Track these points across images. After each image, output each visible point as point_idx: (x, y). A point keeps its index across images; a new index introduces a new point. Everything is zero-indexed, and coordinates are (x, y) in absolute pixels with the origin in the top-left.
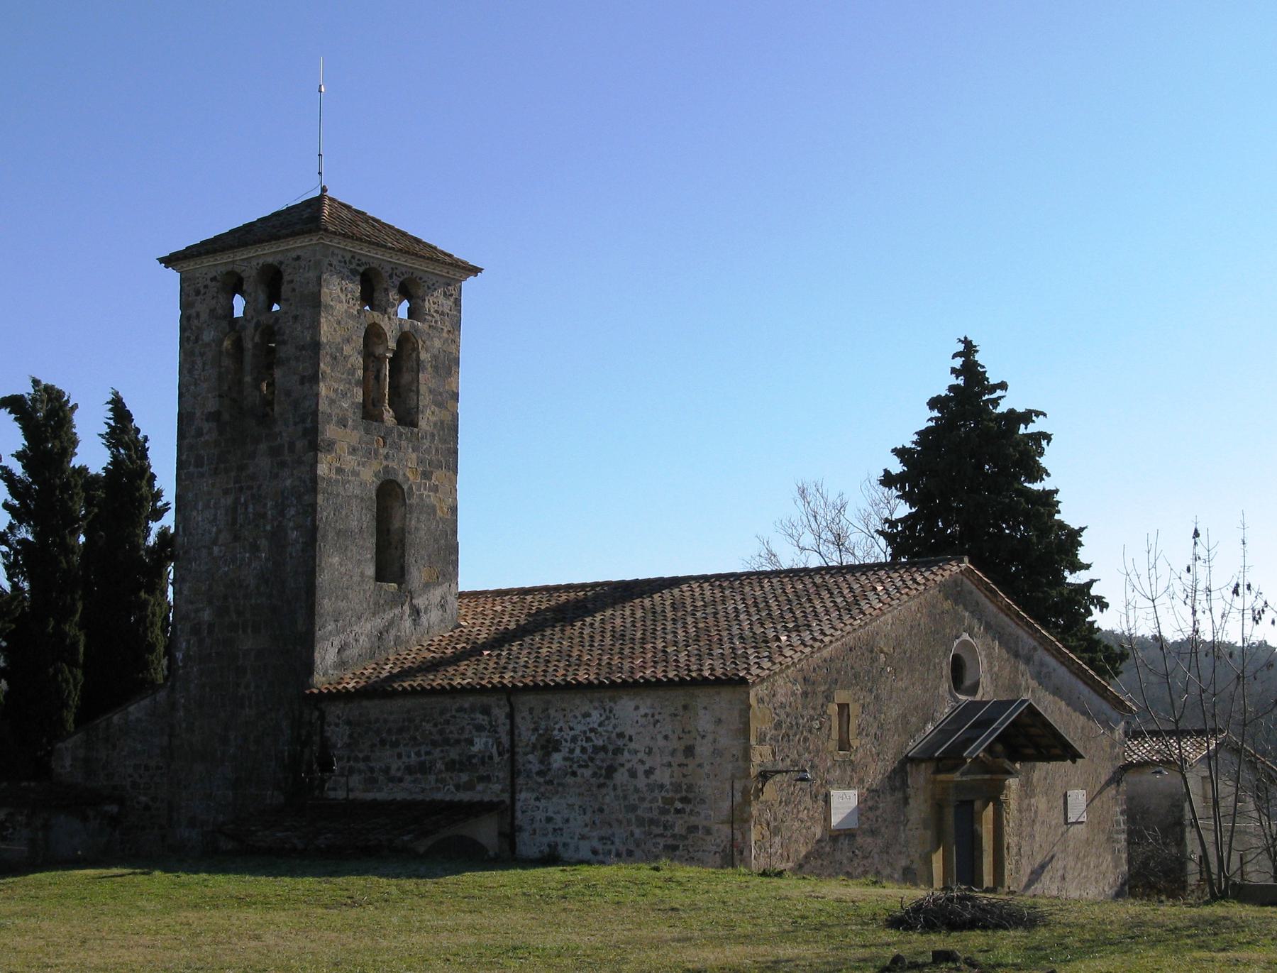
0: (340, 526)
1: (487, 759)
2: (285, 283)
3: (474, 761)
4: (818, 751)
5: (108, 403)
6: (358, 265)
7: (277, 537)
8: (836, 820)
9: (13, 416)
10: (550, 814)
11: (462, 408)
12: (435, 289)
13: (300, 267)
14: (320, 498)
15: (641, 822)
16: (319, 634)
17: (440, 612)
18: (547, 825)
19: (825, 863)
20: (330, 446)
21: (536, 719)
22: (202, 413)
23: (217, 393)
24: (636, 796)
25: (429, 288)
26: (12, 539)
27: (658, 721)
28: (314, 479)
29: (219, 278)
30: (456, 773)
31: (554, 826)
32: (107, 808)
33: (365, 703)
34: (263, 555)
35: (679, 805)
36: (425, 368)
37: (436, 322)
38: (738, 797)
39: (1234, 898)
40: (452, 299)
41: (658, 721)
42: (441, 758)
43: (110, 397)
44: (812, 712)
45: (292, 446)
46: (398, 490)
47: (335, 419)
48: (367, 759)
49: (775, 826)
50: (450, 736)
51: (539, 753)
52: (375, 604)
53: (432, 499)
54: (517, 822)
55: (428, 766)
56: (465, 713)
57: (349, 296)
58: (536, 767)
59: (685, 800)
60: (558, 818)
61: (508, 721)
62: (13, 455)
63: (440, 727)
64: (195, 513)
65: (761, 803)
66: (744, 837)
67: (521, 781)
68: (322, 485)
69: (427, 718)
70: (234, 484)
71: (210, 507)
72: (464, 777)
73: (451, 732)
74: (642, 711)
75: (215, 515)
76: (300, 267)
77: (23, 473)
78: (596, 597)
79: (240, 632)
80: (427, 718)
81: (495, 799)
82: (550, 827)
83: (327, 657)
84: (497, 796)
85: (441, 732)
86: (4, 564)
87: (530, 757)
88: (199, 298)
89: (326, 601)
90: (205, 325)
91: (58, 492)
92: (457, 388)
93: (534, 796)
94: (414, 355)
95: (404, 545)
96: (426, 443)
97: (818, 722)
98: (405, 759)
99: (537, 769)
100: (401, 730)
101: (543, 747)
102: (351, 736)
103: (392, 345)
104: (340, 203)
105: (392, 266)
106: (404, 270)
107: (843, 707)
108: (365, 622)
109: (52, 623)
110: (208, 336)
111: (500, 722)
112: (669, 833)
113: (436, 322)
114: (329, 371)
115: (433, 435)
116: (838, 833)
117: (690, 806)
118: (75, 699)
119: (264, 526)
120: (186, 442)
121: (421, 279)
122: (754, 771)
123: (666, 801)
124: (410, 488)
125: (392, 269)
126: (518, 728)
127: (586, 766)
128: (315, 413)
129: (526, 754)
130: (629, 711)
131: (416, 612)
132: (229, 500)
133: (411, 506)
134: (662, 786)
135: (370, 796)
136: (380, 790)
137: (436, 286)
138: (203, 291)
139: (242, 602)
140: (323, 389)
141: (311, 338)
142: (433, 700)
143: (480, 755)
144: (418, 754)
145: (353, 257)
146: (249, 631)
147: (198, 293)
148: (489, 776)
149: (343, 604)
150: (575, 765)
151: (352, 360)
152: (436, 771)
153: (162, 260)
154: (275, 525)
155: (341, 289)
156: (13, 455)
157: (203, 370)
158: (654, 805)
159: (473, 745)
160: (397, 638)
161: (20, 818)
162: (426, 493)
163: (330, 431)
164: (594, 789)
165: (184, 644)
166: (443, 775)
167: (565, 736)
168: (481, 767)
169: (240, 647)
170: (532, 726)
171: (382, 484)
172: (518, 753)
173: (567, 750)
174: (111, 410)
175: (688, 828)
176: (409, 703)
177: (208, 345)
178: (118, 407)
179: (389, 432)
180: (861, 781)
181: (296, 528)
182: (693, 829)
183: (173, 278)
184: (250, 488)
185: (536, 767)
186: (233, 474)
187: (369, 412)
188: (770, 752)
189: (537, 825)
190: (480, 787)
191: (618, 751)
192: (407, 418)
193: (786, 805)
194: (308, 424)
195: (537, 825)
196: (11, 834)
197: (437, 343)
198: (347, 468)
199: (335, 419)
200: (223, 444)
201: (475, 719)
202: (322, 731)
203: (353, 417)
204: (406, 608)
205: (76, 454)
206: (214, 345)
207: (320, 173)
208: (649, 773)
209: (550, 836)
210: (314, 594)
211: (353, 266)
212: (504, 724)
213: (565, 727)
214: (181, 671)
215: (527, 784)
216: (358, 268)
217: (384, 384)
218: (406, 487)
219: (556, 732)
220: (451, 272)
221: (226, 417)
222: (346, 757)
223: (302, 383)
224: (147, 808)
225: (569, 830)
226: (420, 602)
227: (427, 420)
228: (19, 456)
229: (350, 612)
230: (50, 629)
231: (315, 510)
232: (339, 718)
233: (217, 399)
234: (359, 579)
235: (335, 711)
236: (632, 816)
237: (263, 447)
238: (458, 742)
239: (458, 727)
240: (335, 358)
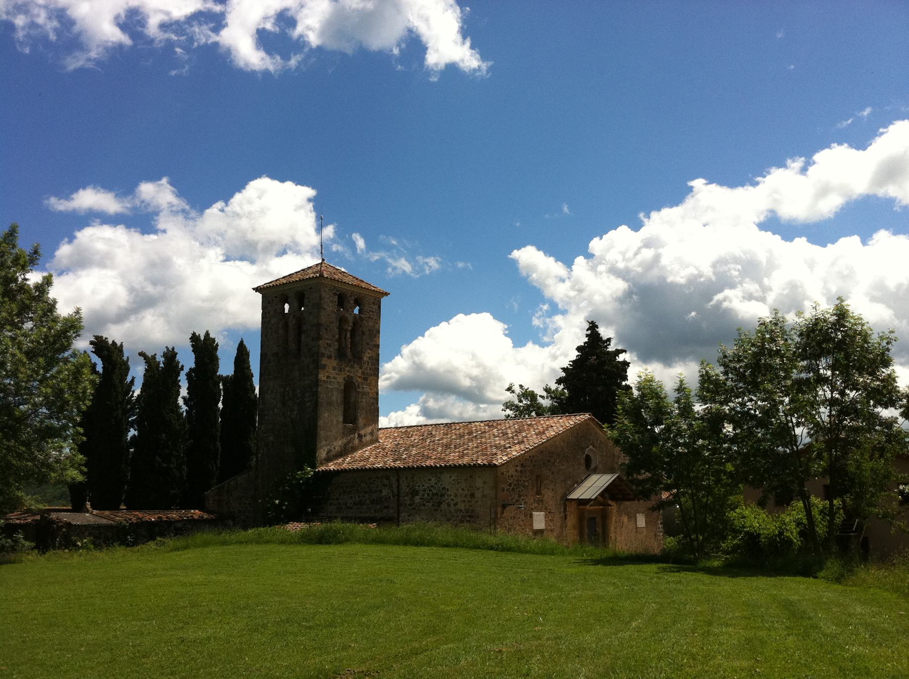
38: (493, 516)
47: (326, 355)
67: (401, 508)
96: (366, 366)
124: (358, 385)
134: (461, 510)
163: (324, 361)
191: (443, 495)
199: (326, 355)
204: (356, 435)
208: (455, 505)
226: (362, 432)
238: (376, 491)
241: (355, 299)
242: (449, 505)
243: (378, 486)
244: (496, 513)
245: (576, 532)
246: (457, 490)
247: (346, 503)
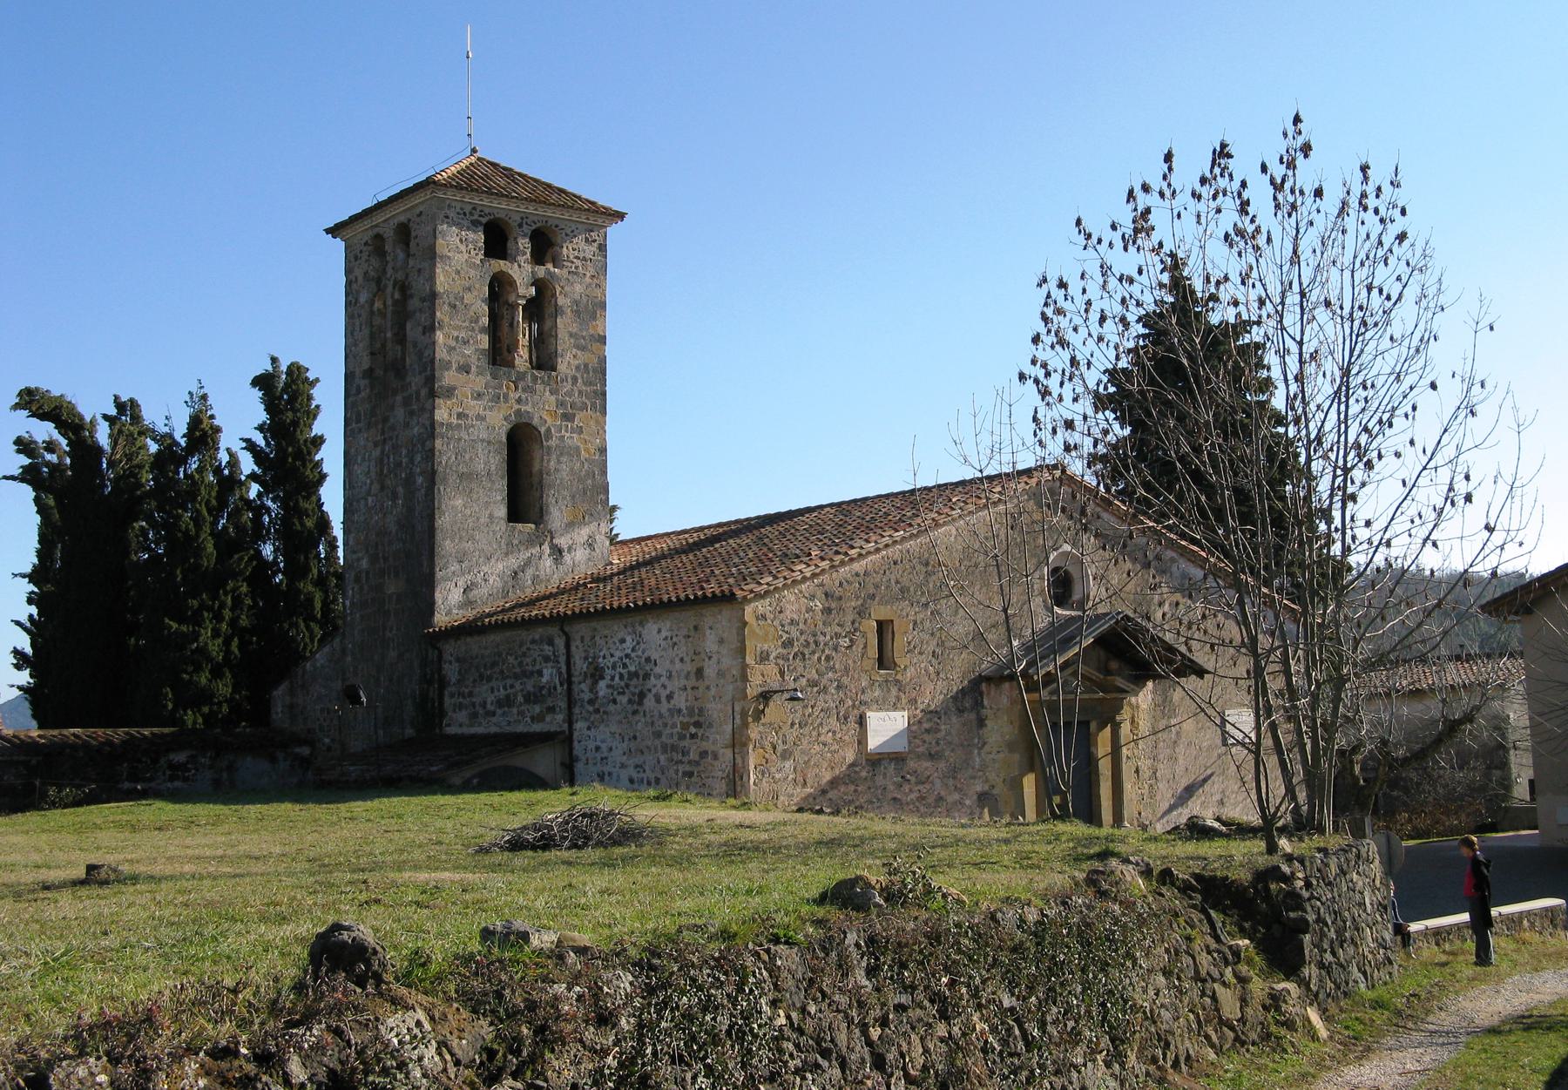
0: (463, 469)
4: (847, 670)
6: (480, 216)
7: (409, 482)
8: (874, 742)
10: (598, 743)
11: (610, 350)
14: (438, 443)
15: (665, 748)
16: (439, 575)
17: (588, 551)
19: (859, 789)
21: (586, 647)
24: (660, 723)
27: (675, 644)
32: (297, 750)
35: (693, 730)
36: (563, 313)
37: (576, 268)
38: (738, 721)
39: (1076, 815)
40: (595, 245)
41: (675, 644)
44: (838, 629)
47: (454, 366)
48: (471, 694)
49: (784, 750)
51: (589, 681)
53: (573, 440)
54: (575, 752)
57: (470, 246)
58: (587, 696)
59: (697, 724)
60: (604, 747)
65: (763, 725)
66: (743, 762)
67: (577, 710)
74: (664, 634)
82: (598, 756)
89: (448, 542)
91: (290, 460)
92: (604, 331)
94: (553, 302)
96: (567, 387)
97: (847, 640)
98: (496, 693)
101: (593, 675)
104: (488, 162)
106: (535, 219)
107: (883, 627)
112: (685, 759)
113: (576, 268)
115: (575, 379)
116: (878, 757)
117: (702, 730)
120: (351, 399)
121: (557, 226)
122: (752, 692)
123: (685, 726)
124: (549, 430)
125: (522, 218)
127: (623, 693)
128: (433, 361)
129: (580, 683)
130: (655, 632)
131: (558, 552)
132: (376, 453)
133: (549, 448)
134: (680, 711)
135: (473, 730)
136: (480, 724)
137: (575, 233)
140: (440, 336)
145: (474, 209)
146: (392, 576)
150: (615, 693)
153: (328, 231)
155: (461, 240)
158: (675, 731)
161: (203, 760)
162: (568, 435)
163: (448, 378)
164: (630, 716)
170: (583, 655)
171: (512, 429)
175: (701, 754)
177: (363, 306)
179: (521, 376)
180: (913, 702)
181: (421, 474)
182: (704, 754)
183: (339, 245)
184: (391, 438)
187: (499, 355)
188: (776, 670)
191: (647, 676)
192: (544, 360)
193: (801, 727)
196: (193, 775)
197: (578, 288)
199: (454, 366)
202: (440, 669)
204: (546, 548)
208: (670, 697)
211: (476, 217)
213: (608, 656)
216: (481, 219)
217: (518, 332)
218: (543, 430)
219: (601, 660)
221: (379, 372)
223: (424, 333)
226: (563, 541)
228: (261, 428)
229: (477, 553)
235: (450, 649)
236: (657, 742)
238: (532, 673)
240: (454, 307)
241: (534, 231)
242: (658, 701)
243: (535, 660)
244: (744, 714)
245: (1017, 757)
246: (672, 662)
247: (485, 703)
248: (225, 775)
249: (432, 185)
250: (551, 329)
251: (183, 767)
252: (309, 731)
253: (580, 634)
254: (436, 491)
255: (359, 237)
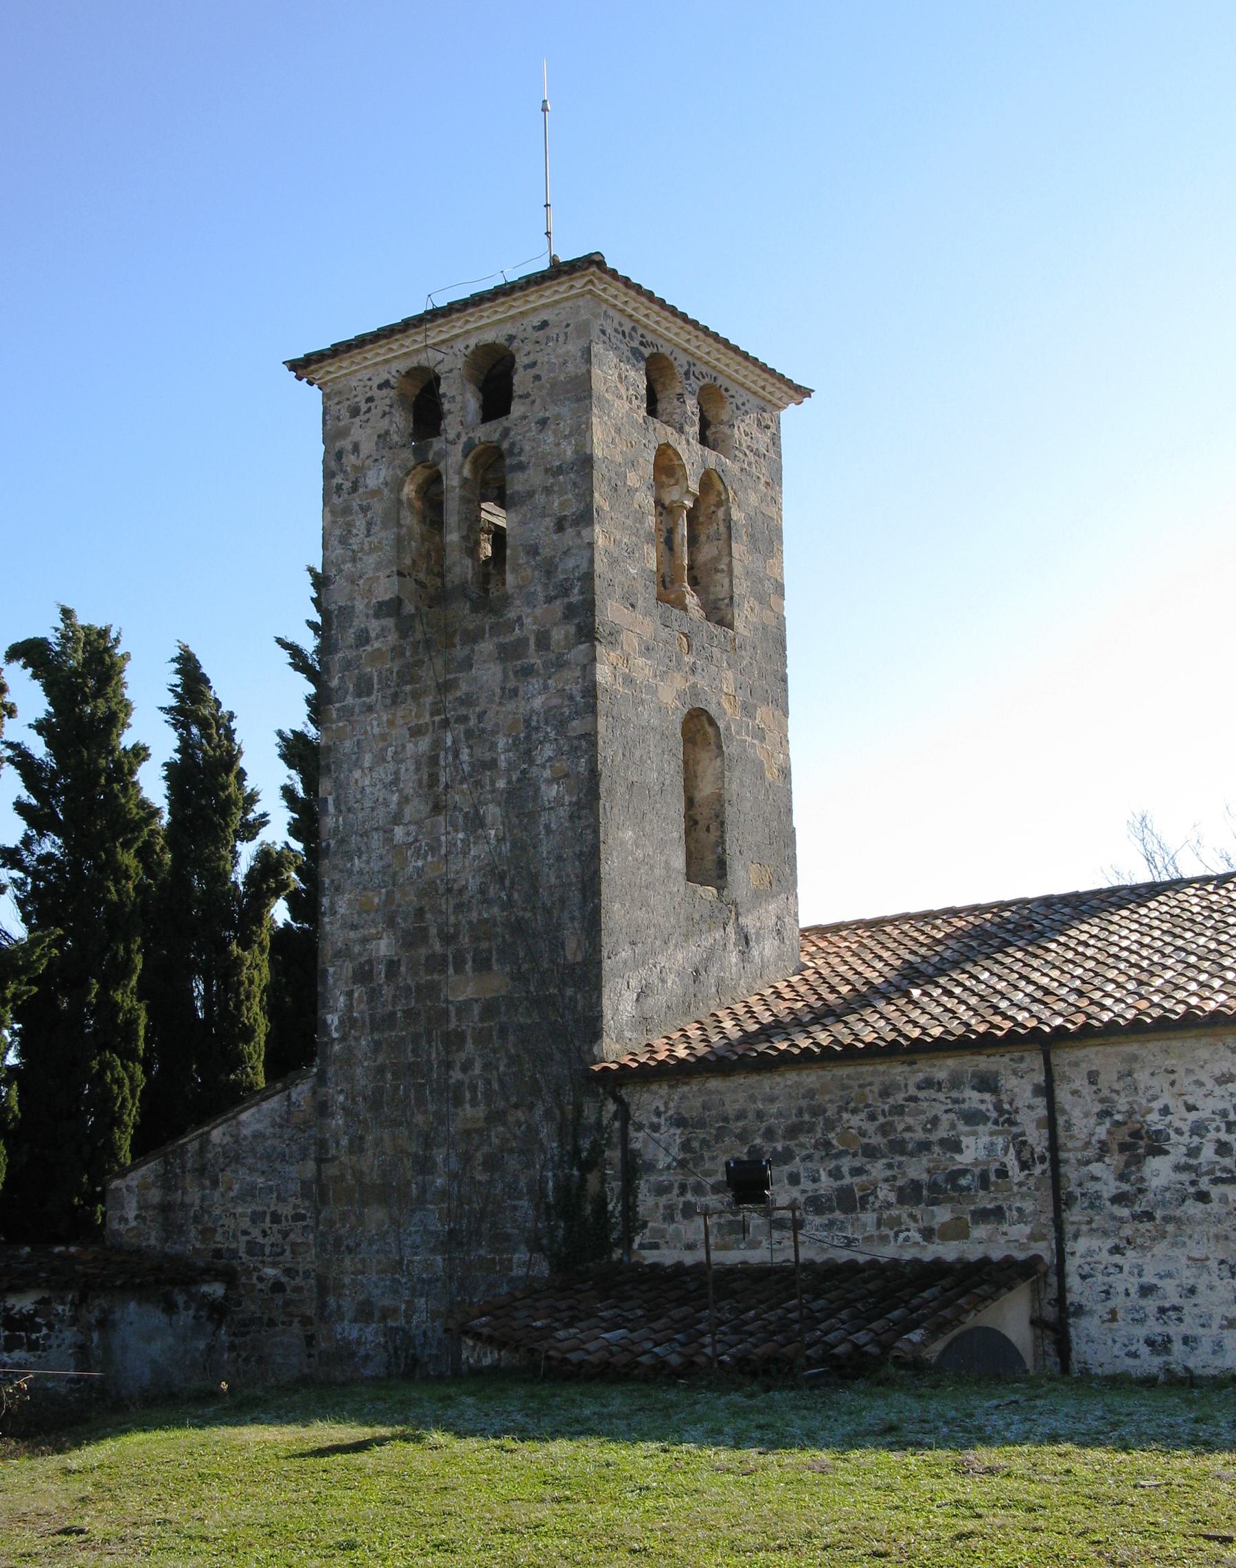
1: (993, 1178)
2: (521, 370)
3: (963, 1182)
5: (173, 660)
6: (642, 344)
9: (30, 670)
10: (1149, 1279)
12: (747, 412)
13: (548, 339)
14: (602, 723)
17: (776, 943)
18: (1143, 1302)
20: (614, 637)
21: (1105, 1093)
22: (367, 606)
23: (395, 569)
25: (738, 408)
26: (29, 860)
28: (591, 691)
29: (393, 381)
30: (922, 1206)
31: (1160, 1303)
32: (205, 1288)
33: (714, 1084)
34: (493, 832)
42: (886, 1180)
43: (176, 653)
45: (543, 641)
46: (710, 730)
50: (907, 1135)
52: (687, 919)
54: (1071, 1298)
55: (858, 1194)
56: (939, 1090)
58: (1110, 1186)
60: (1169, 1286)
61: (1041, 1102)
62: (30, 726)
63: (881, 1120)
64: (357, 774)
67: (1074, 1215)
68: (603, 704)
69: (852, 1105)
70: (432, 715)
71: (384, 760)
72: (943, 1215)
73: (909, 1129)
75: (397, 773)
76: (548, 339)
77: (47, 755)
78: (979, 933)
79: (451, 971)
80: (852, 1105)
81: (1020, 1256)
82: (1151, 1304)
83: (621, 1008)
84: (1022, 1247)
85: (885, 1130)
86: (16, 897)
87: (1096, 1168)
88: (357, 419)
89: (617, 906)
90: (368, 462)
93: (1110, 1243)
94: (721, 513)
95: (722, 823)
98: (806, 1184)
99: (1114, 1191)
100: (793, 1131)
102: (685, 1146)
103: (694, 486)
105: (690, 358)
106: (705, 369)
108: (675, 950)
109: (96, 987)
110: (375, 478)
111: (1019, 1103)
113: (750, 464)
114: (606, 508)
118: (131, 1115)
119: (493, 783)
124: (728, 728)
125: (689, 364)
126: (1064, 1112)
128: (588, 578)
132: (424, 744)
135: (732, 1257)
136: (754, 1245)
138: (364, 407)
139: (452, 919)
141: (576, 452)
142: (865, 1069)
143: (977, 1171)
144: (836, 1174)
146: (469, 967)
147: (355, 412)
148: (999, 1208)
149: (641, 914)
150: (1206, 1179)
151: (639, 496)
152: (877, 1205)
153: (294, 366)
154: (514, 778)
155: (620, 376)
156: (30, 726)
157: (368, 535)
159: (960, 1151)
160: (720, 983)
161: (60, 1308)
162: (749, 739)
163: (610, 611)
165: (342, 999)
166: (894, 1212)
167: (1177, 1124)
168: (982, 1193)
169: (451, 998)
170: (1097, 1108)
172: (1067, 1161)
173: (1184, 1150)
174: (178, 672)
176: (810, 1078)
177: (376, 493)
178: (188, 666)
183: (309, 399)
185: (1110, 1186)
186: (429, 700)
189: (1118, 1301)
190: (980, 1231)
194: (575, 597)
195: (1118, 1301)
196: (46, 1337)
198: (638, 677)
200: (408, 654)
201: (964, 1101)
202: (625, 1139)
203: (647, 594)
205: (130, 726)
206: (386, 491)
207: (548, 233)
209: (1151, 1321)
210: (597, 893)
211: (635, 344)
212: (1030, 1107)
214: (337, 1047)
215: (1090, 1222)
216: (642, 348)
219: (1153, 1117)
220: (769, 388)
221: (409, 608)
222: (676, 1185)
224: (278, 1287)
225: (1196, 1311)
226: (748, 921)
227: (745, 617)
228: (41, 727)
229: (653, 930)
230: (92, 997)
231: (594, 744)
232: (658, 1114)
233: (395, 578)
234: (663, 872)
237: (486, 647)
238: (925, 1146)
239: (922, 1117)
248: (95, 1336)
249: (593, 269)
250: (717, 559)
251: (25, 1322)
252: (218, 1253)
253: (1085, 1067)
254: (601, 811)
255: (365, 374)
